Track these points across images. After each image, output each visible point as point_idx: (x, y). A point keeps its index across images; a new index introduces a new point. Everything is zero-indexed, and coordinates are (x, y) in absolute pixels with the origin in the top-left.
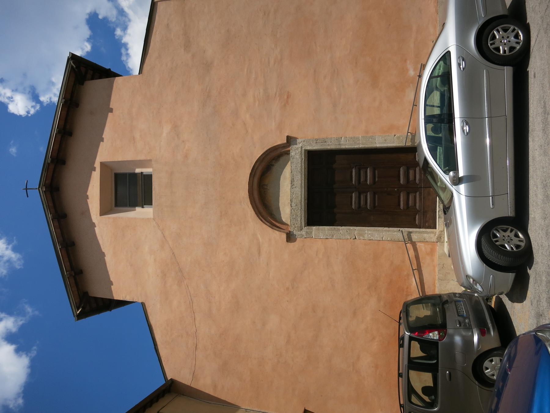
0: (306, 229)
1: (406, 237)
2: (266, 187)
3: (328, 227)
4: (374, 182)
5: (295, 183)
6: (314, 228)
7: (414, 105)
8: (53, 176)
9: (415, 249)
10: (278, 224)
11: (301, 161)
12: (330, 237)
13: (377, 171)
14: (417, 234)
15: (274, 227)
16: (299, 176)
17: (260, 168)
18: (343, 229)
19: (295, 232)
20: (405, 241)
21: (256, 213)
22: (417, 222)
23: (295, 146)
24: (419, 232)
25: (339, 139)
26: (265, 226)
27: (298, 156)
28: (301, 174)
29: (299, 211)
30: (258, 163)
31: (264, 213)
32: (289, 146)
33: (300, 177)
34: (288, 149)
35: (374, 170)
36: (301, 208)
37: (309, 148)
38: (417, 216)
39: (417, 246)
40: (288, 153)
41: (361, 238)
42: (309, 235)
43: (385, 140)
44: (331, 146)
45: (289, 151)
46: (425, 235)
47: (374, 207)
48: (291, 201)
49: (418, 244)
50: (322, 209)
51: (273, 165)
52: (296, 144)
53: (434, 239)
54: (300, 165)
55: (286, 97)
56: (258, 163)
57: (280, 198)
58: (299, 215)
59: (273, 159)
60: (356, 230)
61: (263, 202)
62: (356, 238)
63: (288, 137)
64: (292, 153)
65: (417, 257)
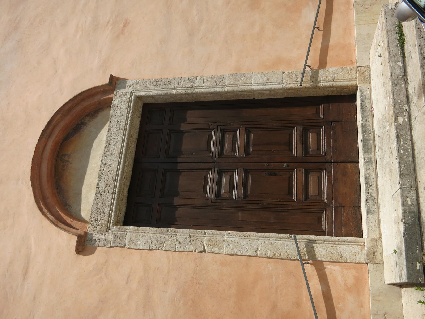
0: (115, 229)
1: (303, 251)
2: (66, 158)
4: (247, 153)
5: (111, 148)
7: (314, 27)
9: (323, 278)
10: (69, 220)
11: (128, 114)
12: (158, 246)
13: (252, 136)
14: (325, 247)
15: (60, 224)
16: (120, 137)
17: (62, 124)
18: (182, 235)
19: (95, 234)
20: (302, 260)
21: (35, 198)
22: (324, 227)
23: (123, 90)
24: (330, 242)
25: (192, 79)
26: (46, 222)
28: (124, 133)
29: (109, 196)
30: (59, 116)
31: (51, 200)
34: (110, 96)
35: (248, 132)
36: (114, 191)
37: (142, 93)
38: (324, 215)
39: (327, 272)
40: (108, 104)
41: (216, 249)
43: (268, 79)
44: (179, 89)
45: (111, 99)
46: (343, 247)
47: (245, 195)
48: (100, 178)
49: (329, 268)
50: (148, 201)
51: (85, 124)
52: (125, 88)
53: (362, 257)
54: (124, 119)
55: (121, 26)
56: (59, 116)
57: (86, 177)
58: (108, 204)
60: (207, 236)
61: (54, 180)
62: (204, 251)
63: (112, 77)
64: (116, 102)
65: (327, 296)
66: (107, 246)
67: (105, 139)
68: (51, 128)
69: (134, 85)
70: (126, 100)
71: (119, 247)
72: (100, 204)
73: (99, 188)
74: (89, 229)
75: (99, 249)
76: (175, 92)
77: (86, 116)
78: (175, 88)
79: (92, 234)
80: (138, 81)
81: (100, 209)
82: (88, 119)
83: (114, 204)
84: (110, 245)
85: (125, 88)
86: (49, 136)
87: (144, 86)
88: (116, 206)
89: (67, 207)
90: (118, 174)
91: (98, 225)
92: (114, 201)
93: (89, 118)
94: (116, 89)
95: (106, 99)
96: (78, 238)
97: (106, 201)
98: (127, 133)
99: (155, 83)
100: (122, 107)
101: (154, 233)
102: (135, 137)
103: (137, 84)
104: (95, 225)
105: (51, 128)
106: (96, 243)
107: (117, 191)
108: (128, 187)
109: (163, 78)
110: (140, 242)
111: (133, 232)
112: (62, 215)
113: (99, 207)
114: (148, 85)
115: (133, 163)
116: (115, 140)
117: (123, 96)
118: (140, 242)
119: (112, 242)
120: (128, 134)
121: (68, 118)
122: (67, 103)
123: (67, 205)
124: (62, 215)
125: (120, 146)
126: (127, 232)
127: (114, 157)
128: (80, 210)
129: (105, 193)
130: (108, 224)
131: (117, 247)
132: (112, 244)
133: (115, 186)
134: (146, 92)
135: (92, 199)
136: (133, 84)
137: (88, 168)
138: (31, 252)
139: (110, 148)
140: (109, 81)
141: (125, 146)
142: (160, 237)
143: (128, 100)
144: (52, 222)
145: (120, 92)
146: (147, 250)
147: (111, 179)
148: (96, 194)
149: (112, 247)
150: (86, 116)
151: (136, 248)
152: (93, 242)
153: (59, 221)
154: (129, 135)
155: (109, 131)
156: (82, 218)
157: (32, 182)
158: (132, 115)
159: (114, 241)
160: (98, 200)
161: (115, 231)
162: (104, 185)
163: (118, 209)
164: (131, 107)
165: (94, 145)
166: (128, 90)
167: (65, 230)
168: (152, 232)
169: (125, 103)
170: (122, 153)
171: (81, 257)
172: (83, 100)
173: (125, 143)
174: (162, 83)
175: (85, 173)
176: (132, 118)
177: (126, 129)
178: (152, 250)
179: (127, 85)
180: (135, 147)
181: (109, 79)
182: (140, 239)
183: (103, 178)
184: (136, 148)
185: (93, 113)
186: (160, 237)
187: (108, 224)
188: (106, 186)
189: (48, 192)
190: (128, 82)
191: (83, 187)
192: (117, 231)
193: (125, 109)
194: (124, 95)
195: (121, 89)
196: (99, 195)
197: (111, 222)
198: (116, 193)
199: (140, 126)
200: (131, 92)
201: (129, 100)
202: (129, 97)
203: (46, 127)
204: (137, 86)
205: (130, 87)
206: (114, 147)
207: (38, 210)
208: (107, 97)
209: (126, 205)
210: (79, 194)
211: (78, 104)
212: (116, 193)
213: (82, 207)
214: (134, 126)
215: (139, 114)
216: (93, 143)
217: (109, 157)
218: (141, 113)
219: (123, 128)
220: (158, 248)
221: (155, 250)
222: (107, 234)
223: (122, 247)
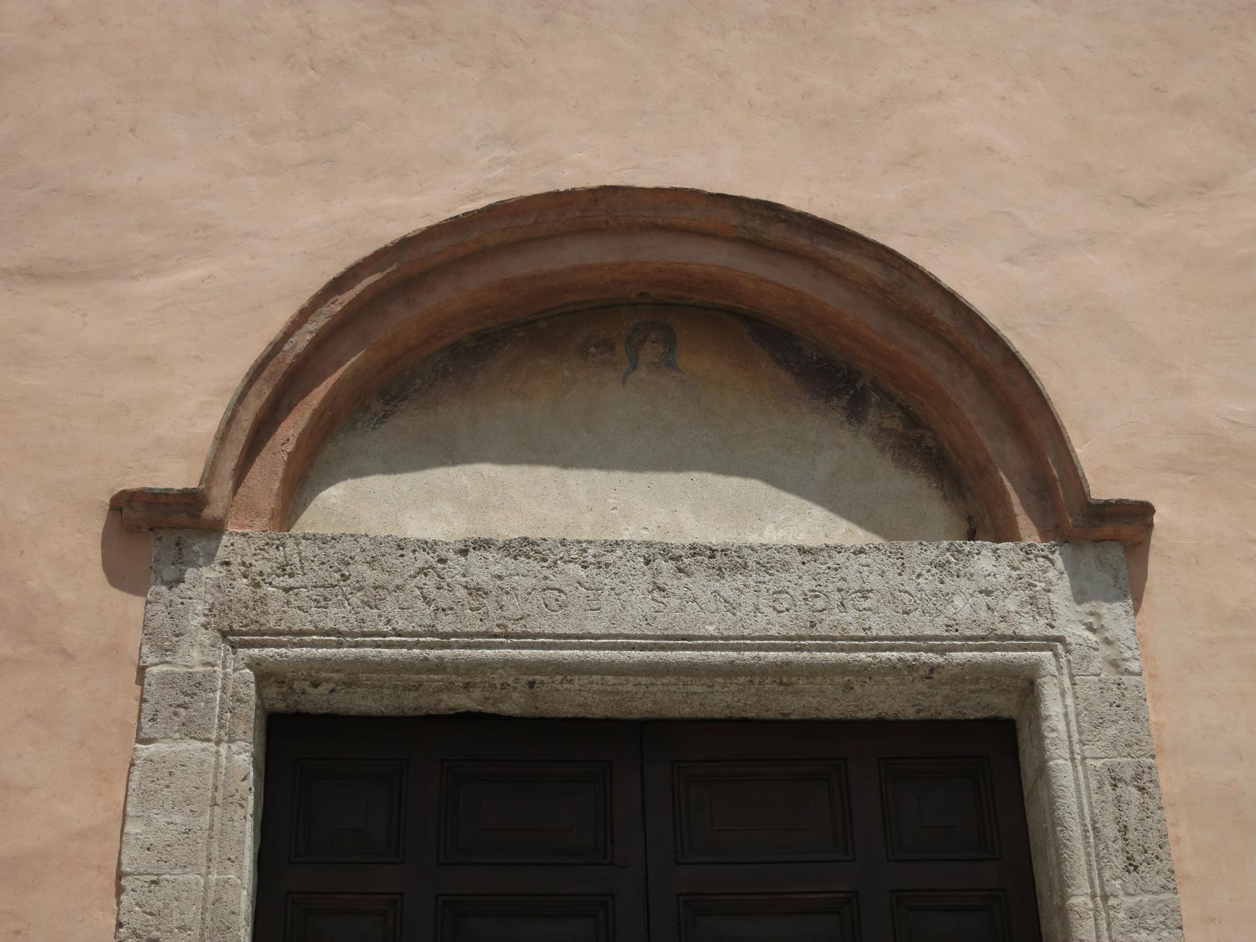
0: (234, 675)
2: (650, 352)
3: (243, 901)
5: (701, 583)
6: (241, 758)
8: (671, 304)
10: (291, 430)
15: (263, 391)
17: (830, 296)
19: (211, 573)
21: (405, 244)
23: (1063, 587)
27: (963, 607)
28: (795, 642)
29: (422, 616)
31: (402, 320)
32: (1055, 531)
33: (758, 625)
34: (1024, 523)
36: (445, 640)
37: (1056, 707)
40: (983, 522)
42: (169, 705)
45: (1002, 531)
48: (524, 548)
51: (856, 412)
52: (1080, 596)
54: (878, 626)
56: (871, 269)
57: (546, 473)
59: (912, 420)
63: (1140, 514)
64: (987, 560)
66: (145, 649)
67: (772, 535)
68: (801, 241)
69: (1105, 650)
70: (1003, 619)
71: (140, 710)
72: (371, 576)
73: (464, 552)
74: (240, 542)
75: (134, 606)
76: (1080, 899)
77: (904, 410)
78: (1105, 898)
79: (210, 557)
80: (1134, 666)
81: (345, 578)
82: (888, 423)
83: (370, 652)
84: (151, 659)
85: (1079, 602)
86: (756, 244)
87: (1104, 708)
88: (362, 662)
89: (377, 406)
90: (543, 646)
91: (257, 585)
92: (389, 645)
93: (896, 424)
94: (1068, 548)
95: (1006, 503)
96: (185, 493)
97: (390, 606)
98: (791, 655)
99: (1128, 774)
100: (958, 601)
101: (206, 887)
102: (795, 706)
103: (1114, 664)
104: (259, 565)
105: (801, 241)
106: (164, 588)
107: (447, 653)
108: (490, 709)
109: (1168, 814)
110: (162, 820)
111: (215, 776)
112: (319, 394)
113: (360, 569)
114: (1112, 731)
115: (636, 715)
116: (748, 598)
117: (1024, 595)
118: (162, 820)
119: (164, 668)
120: (788, 663)
121: (870, 320)
122: (950, 297)
123: (387, 403)
124: (319, 394)
125: (711, 629)
126: (218, 743)
127: (648, 606)
128: (358, 473)
129: (433, 593)
130: (263, 636)
131: (143, 700)
132: (155, 670)
133: (472, 639)
134: (1062, 726)
135: (416, 527)
136: (1108, 642)
137: (597, 475)
138: (134, 278)
139: (701, 576)
140: (1107, 504)
141: (716, 656)
142: (183, 928)
143: (1003, 628)
144: (276, 348)
145: (1051, 574)
146: (119, 864)
147: (514, 607)
148: (427, 546)
149: (142, 670)
150: (904, 410)
151: (133, 799)
152: (169, 572)
153: (279, 382)
154: (785, 668)
155: (802, 550)
156: (315, 493)
157: (490, 210)
158: (911, 667)
159: (168, 681)
160: (393, 560)
161: (225, 676)
162: (481, 577)
163: (353, 673)
164: (959, 657)
165: (735, 481)
166: (1070, 622)
167: (230, 420)
168: (214, 877)
169: (983, 614)
170: (672, 648)
171: (97, 525)
172: (985, 378)
173: (733, 655)
174: (1132, 816)
175: (566, 464)
176: (892, 668)
177: (821, 649)
178: (120, 890)
179: (1104, 608)
180: (736, 714)
181: (1120, 503)
182: (178, 818)
183: (523, 564)
184: (729, 721)
185: (931, 443)
186: (183, 928)
187: (263, 636)
188: (476, 591)
189: (444, 297)
190: (1119, 608)
191: (487, 469)
192: (224, 689)
193: (941, 620)
194: (1033, 600)
195: (1073, 576)
196: (423, 558)
197: (271, 651)
198: (434, 653)
199: (866, 722)
200: (1061, 639)
201: (1002, 637)
202: (1026, 630)
203: (802, 216)
204: (1096, 665)
205: (1090, 628)
206: (703, 599)
207: (335, 268)
208: (1018, 508)
209: (390, 711)
210: (450, 453)
211: (957, 353)
212: (434, 653)
213: (376, 484)
214: (848, 687)
215: (939, 704)
216: (745, 473)
217: (642, 583)
218: (948, 714)
219: (822, 630)
220: (124, 919)
221: (119, 903)
222: (206, 637)
223: (139, 729)
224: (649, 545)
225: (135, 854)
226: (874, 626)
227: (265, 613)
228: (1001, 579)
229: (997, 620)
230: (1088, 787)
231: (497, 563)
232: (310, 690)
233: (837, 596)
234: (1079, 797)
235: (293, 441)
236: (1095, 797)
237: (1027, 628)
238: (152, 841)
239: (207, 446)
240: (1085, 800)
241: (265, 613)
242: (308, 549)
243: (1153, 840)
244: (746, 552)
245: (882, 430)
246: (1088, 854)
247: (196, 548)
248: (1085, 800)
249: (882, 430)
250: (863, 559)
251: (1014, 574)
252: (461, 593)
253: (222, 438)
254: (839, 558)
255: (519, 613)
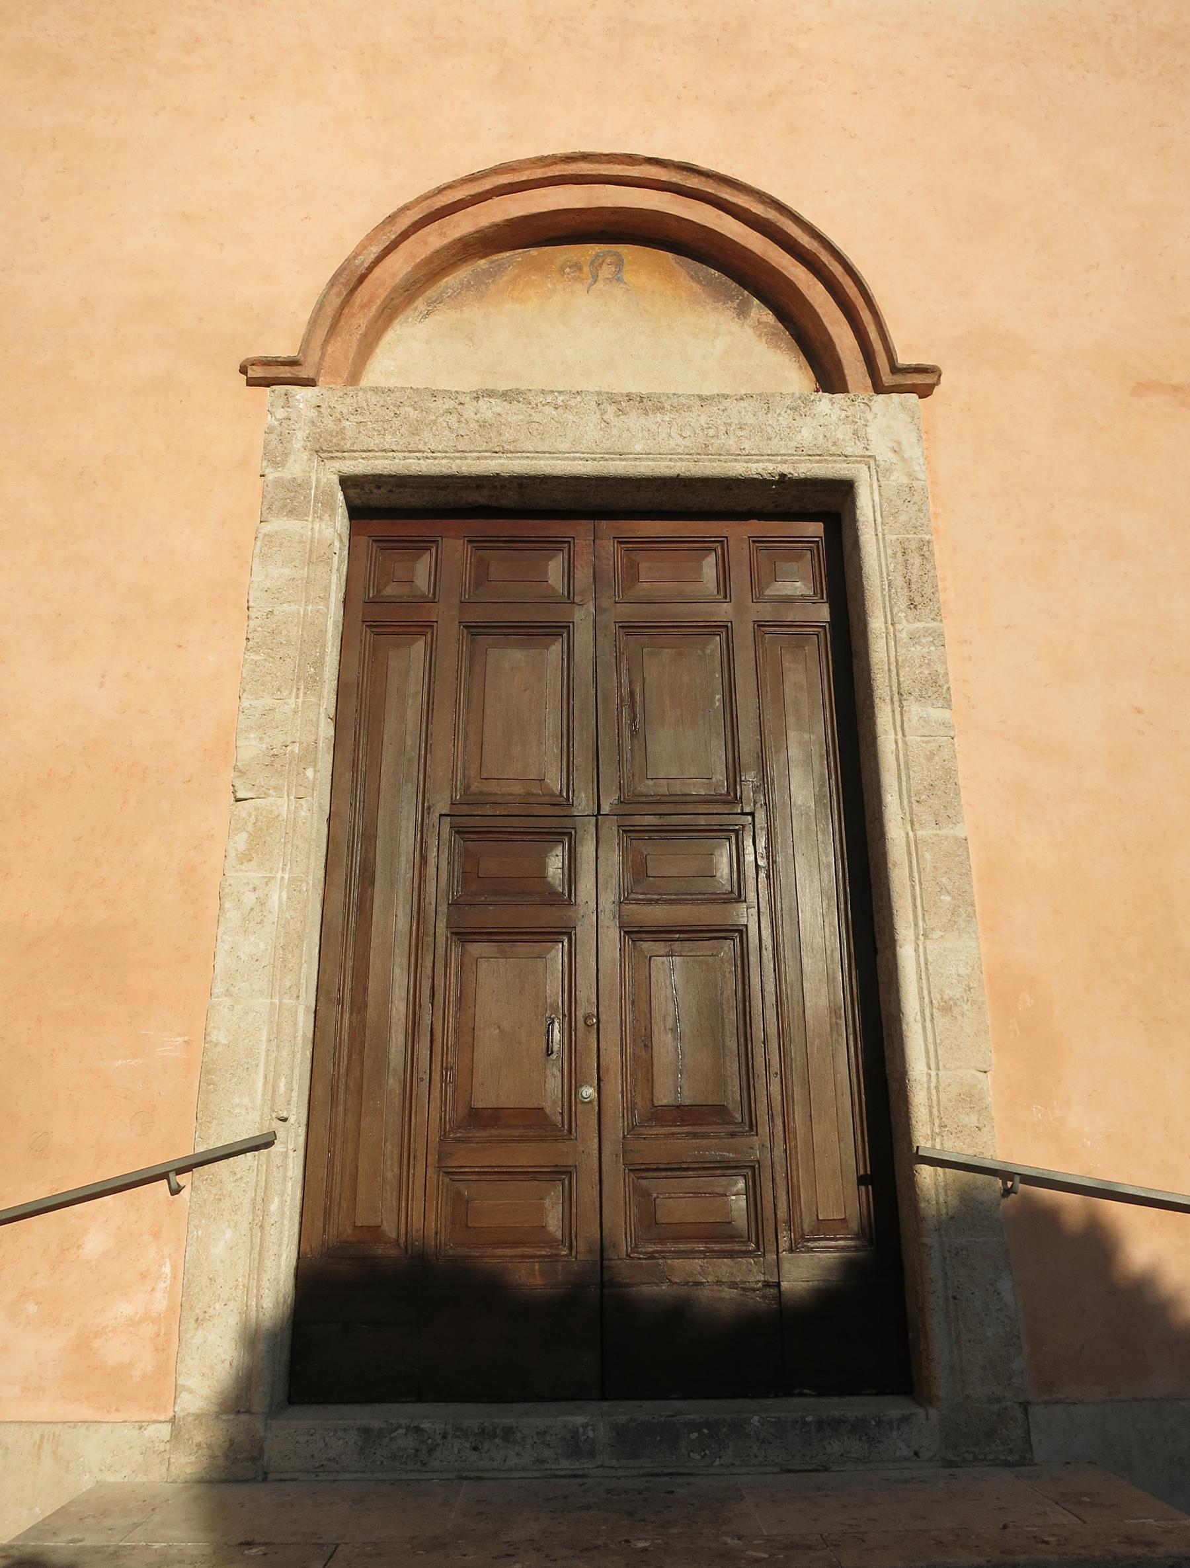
2: (606, 271)
5: (634, 420)
70: (834, 444)
99: (913, 546)
108: (495, 504)
109: (939, 573)
139: (633, 415)
159: (279, 483)
187: (340, 452)
188: (483, 425)
196: (449, 404)
224: (599, 394)
225: (259, 594)
226: (747, 447)
227: (344, 439)
228: (834, 418)
229: (830, 444)
230: (886, 554)
231: (498, 406)
232: (375, 491)
233: (723, 429)
234: (880, 560)
235: (363, 327)
236: (890, 560)
237: (849, 449)
238: (269, 585)
239: (301, 330)
240: (883, 562)
241: (344, 439)
242: (373, 399)
243: (928, 590)
244: (663, 399)
245: (760, 323)
246: (883, 596)
247: (298, 397)
248: (883, 562)
249: (760, 323)
250: (742, 404)
251: (844, 413)
252: (473, 425)
253: (313, 323)
254: (726, 403)
255: (512, 438)
